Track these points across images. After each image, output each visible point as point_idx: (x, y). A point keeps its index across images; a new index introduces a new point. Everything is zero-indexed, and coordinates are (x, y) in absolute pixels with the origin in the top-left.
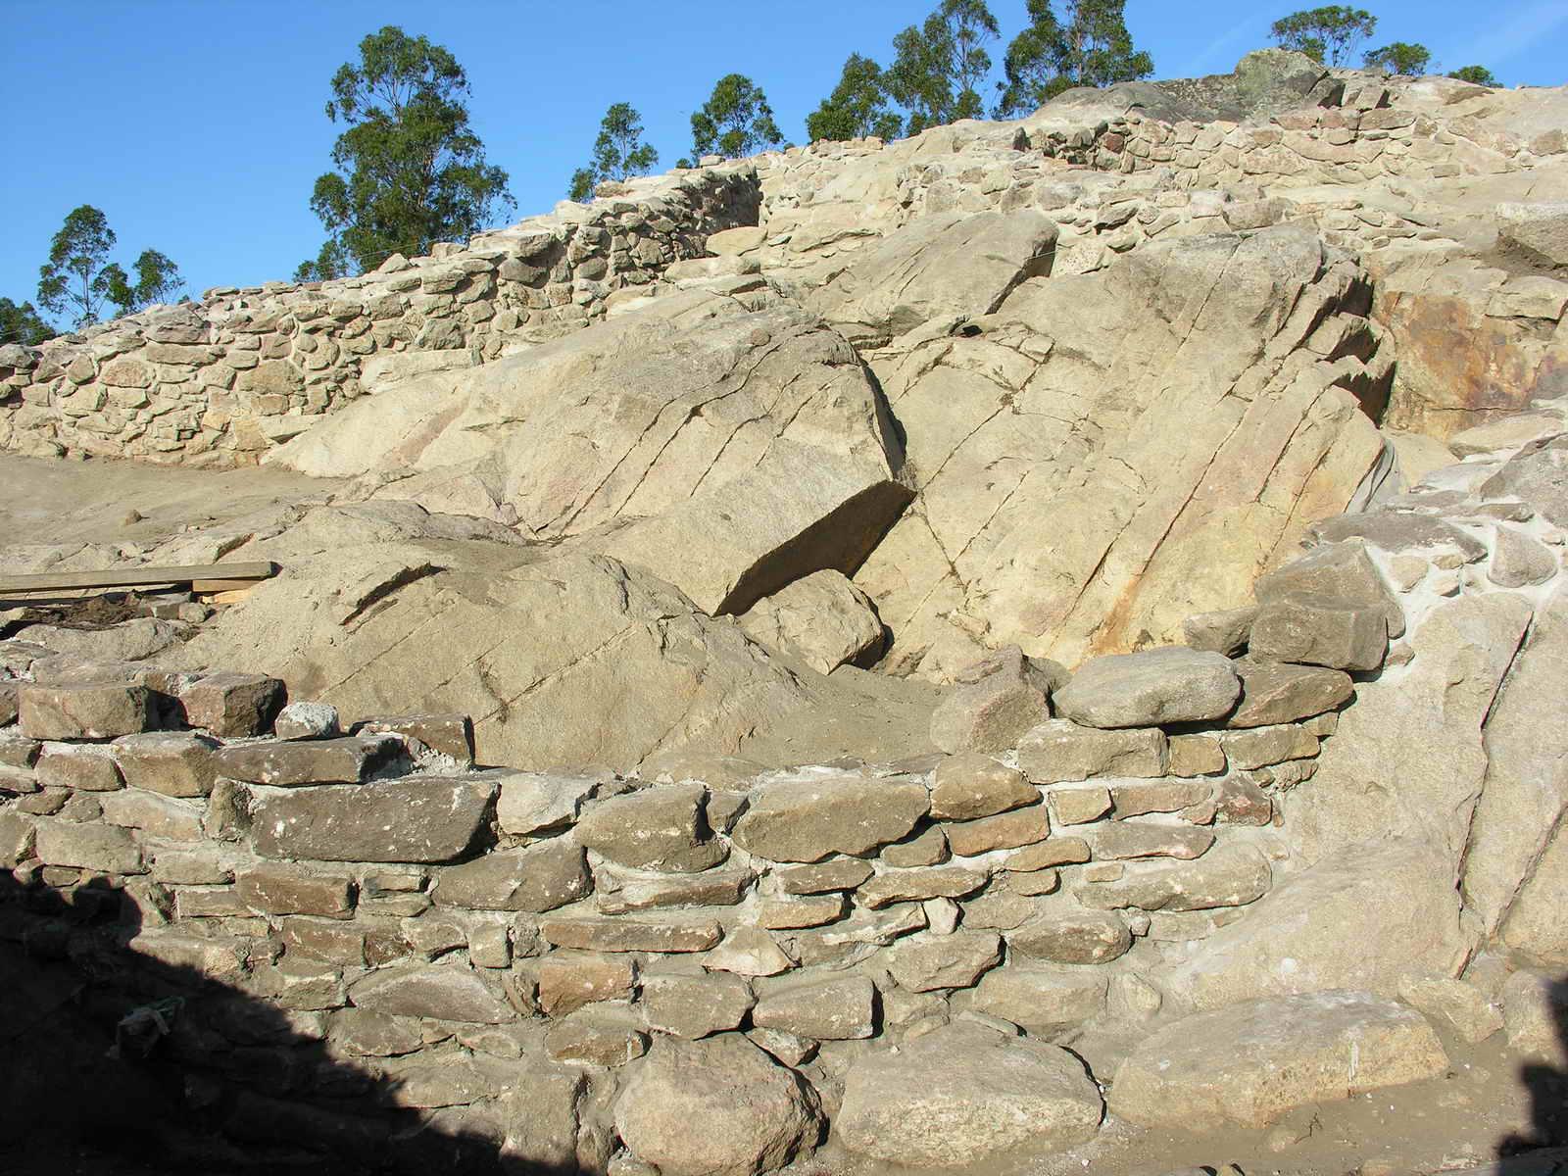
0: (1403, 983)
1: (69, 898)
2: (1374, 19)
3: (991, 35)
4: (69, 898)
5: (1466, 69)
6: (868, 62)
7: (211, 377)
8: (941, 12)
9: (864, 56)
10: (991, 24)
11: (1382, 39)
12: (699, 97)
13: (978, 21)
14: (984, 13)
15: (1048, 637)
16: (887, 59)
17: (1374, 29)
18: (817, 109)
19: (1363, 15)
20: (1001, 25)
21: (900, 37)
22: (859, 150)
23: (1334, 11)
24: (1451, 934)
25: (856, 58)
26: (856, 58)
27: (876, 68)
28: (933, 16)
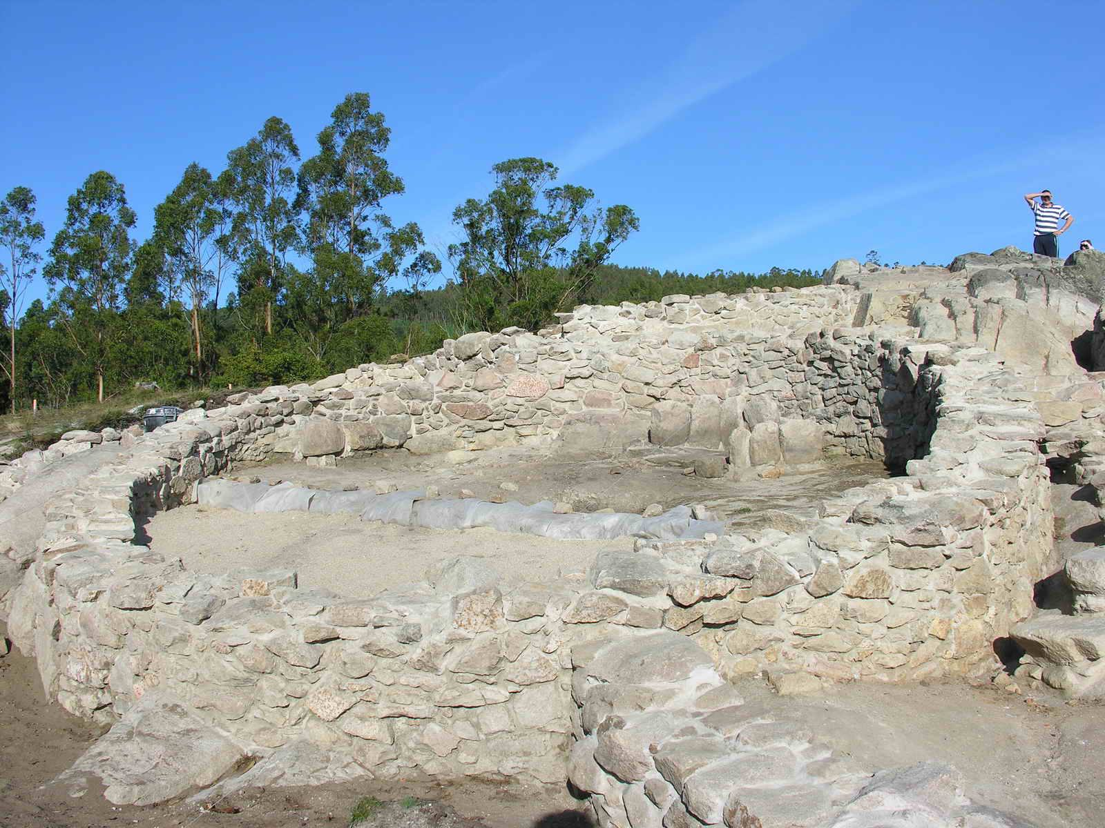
0: (283, 593)
1: (145, 526)
2: (557, 169)
3: (294, 158)
4: (145, 526)
5: (617, 206)
6: (204, 171)
7: (942, 581)
8: (259, 138)
9: (201, 166)
10: (294, 151)
11: (560, 182)
12: (76, 184)
13: (287, 148)
14: (291, 142)
15: (217, 227)
16: (217, 168)
17: (558, 175)
18: (163, 201)
19: (550, 166)
20: (300, 152)
21: (232, 152)
22: (224, 423)
23: (533, 160)
24: (328, 651)
25: (195, 166)
26: (195, 166)
27: (209, 176)
28: (253, 140)
